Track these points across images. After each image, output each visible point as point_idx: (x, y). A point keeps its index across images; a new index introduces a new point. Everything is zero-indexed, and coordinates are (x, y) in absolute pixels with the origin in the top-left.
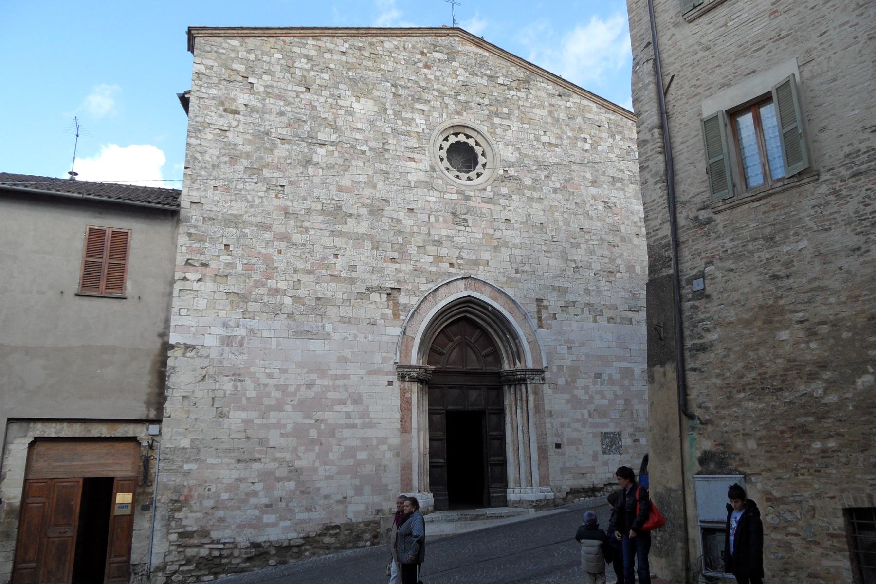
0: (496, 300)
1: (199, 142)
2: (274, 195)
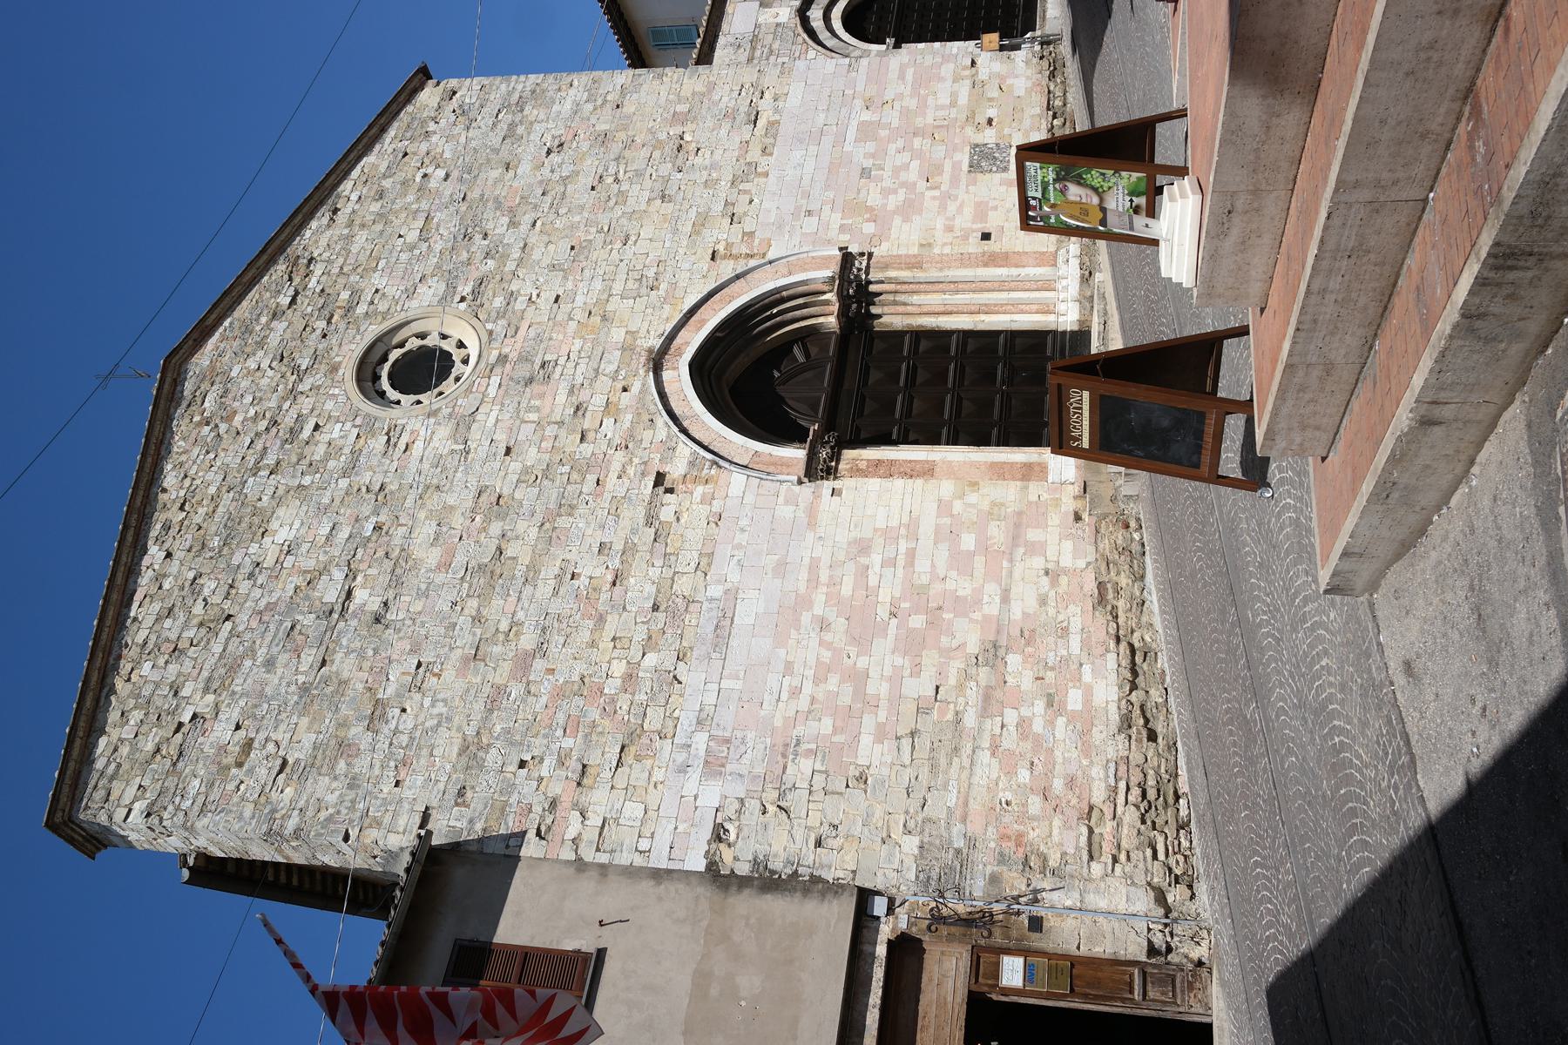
1: (296, 812)
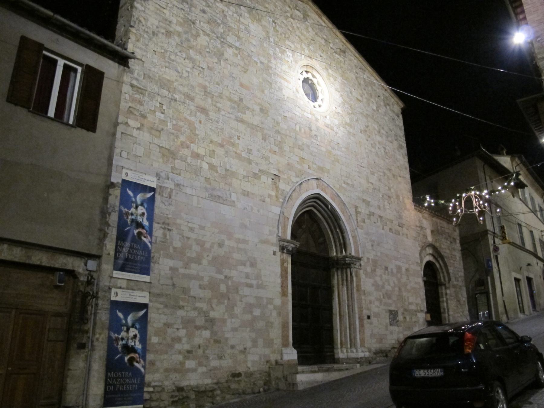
0: (334, 200)
1: (143, 9)
2: (197, 74)
